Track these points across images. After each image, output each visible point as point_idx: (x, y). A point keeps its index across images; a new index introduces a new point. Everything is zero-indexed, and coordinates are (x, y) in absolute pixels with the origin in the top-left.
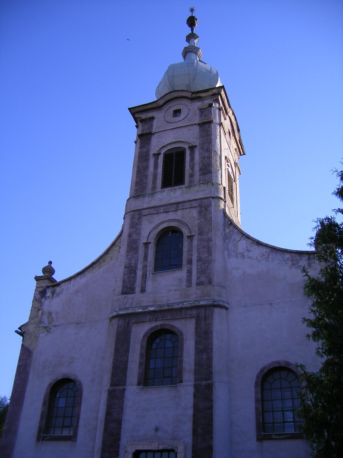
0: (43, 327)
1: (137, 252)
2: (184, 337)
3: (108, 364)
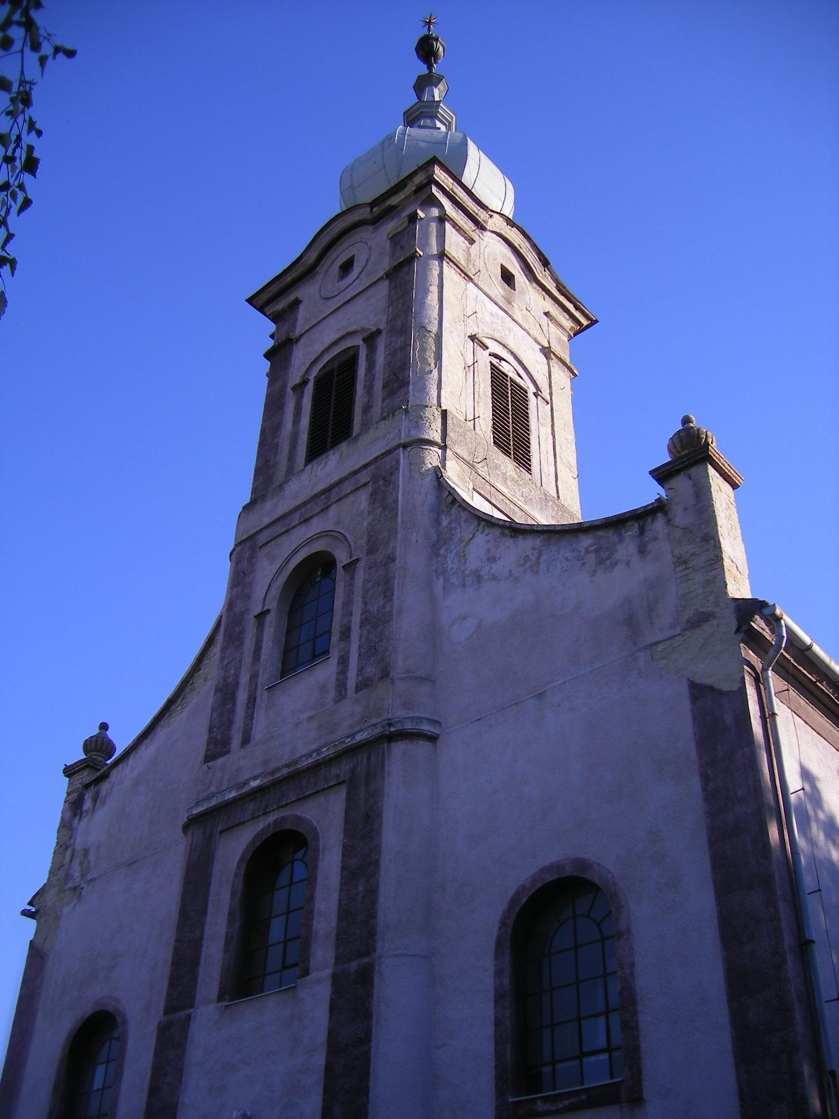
0: (70, 889)
1: (242, 644)
2: (321, 842)
3: (165, 954)
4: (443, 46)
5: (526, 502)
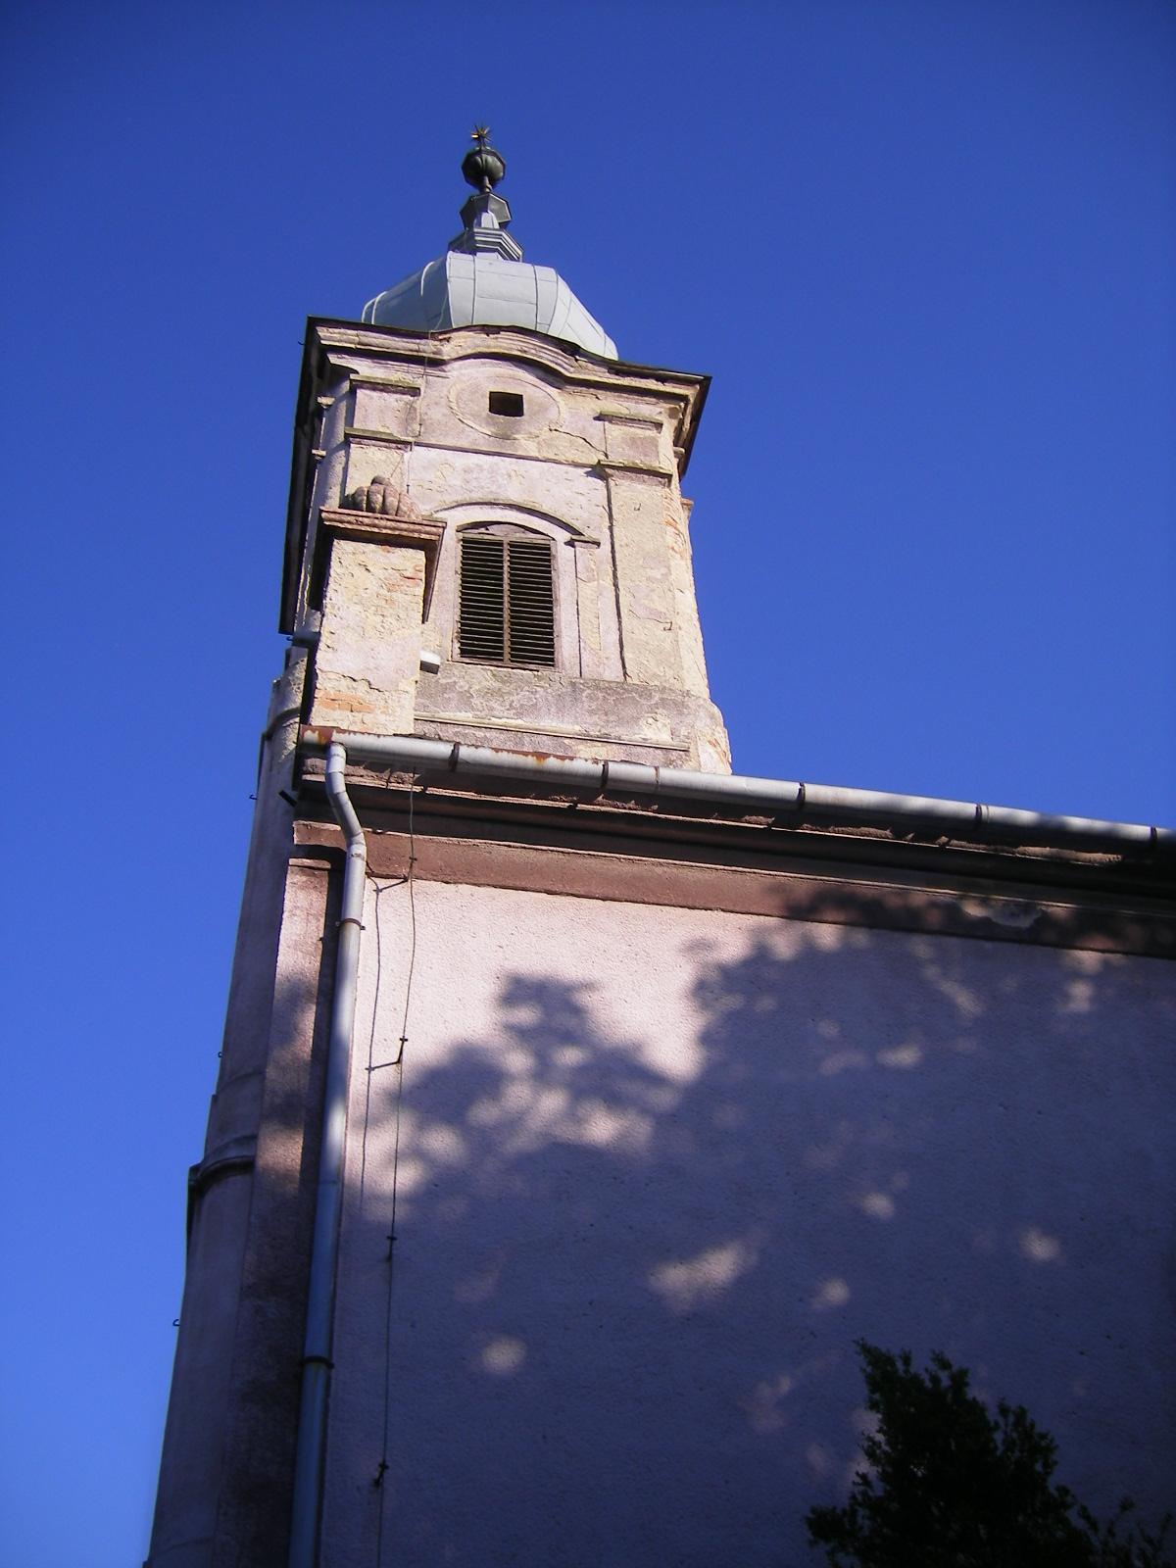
4: (494, 154)
5: (519, 715)
